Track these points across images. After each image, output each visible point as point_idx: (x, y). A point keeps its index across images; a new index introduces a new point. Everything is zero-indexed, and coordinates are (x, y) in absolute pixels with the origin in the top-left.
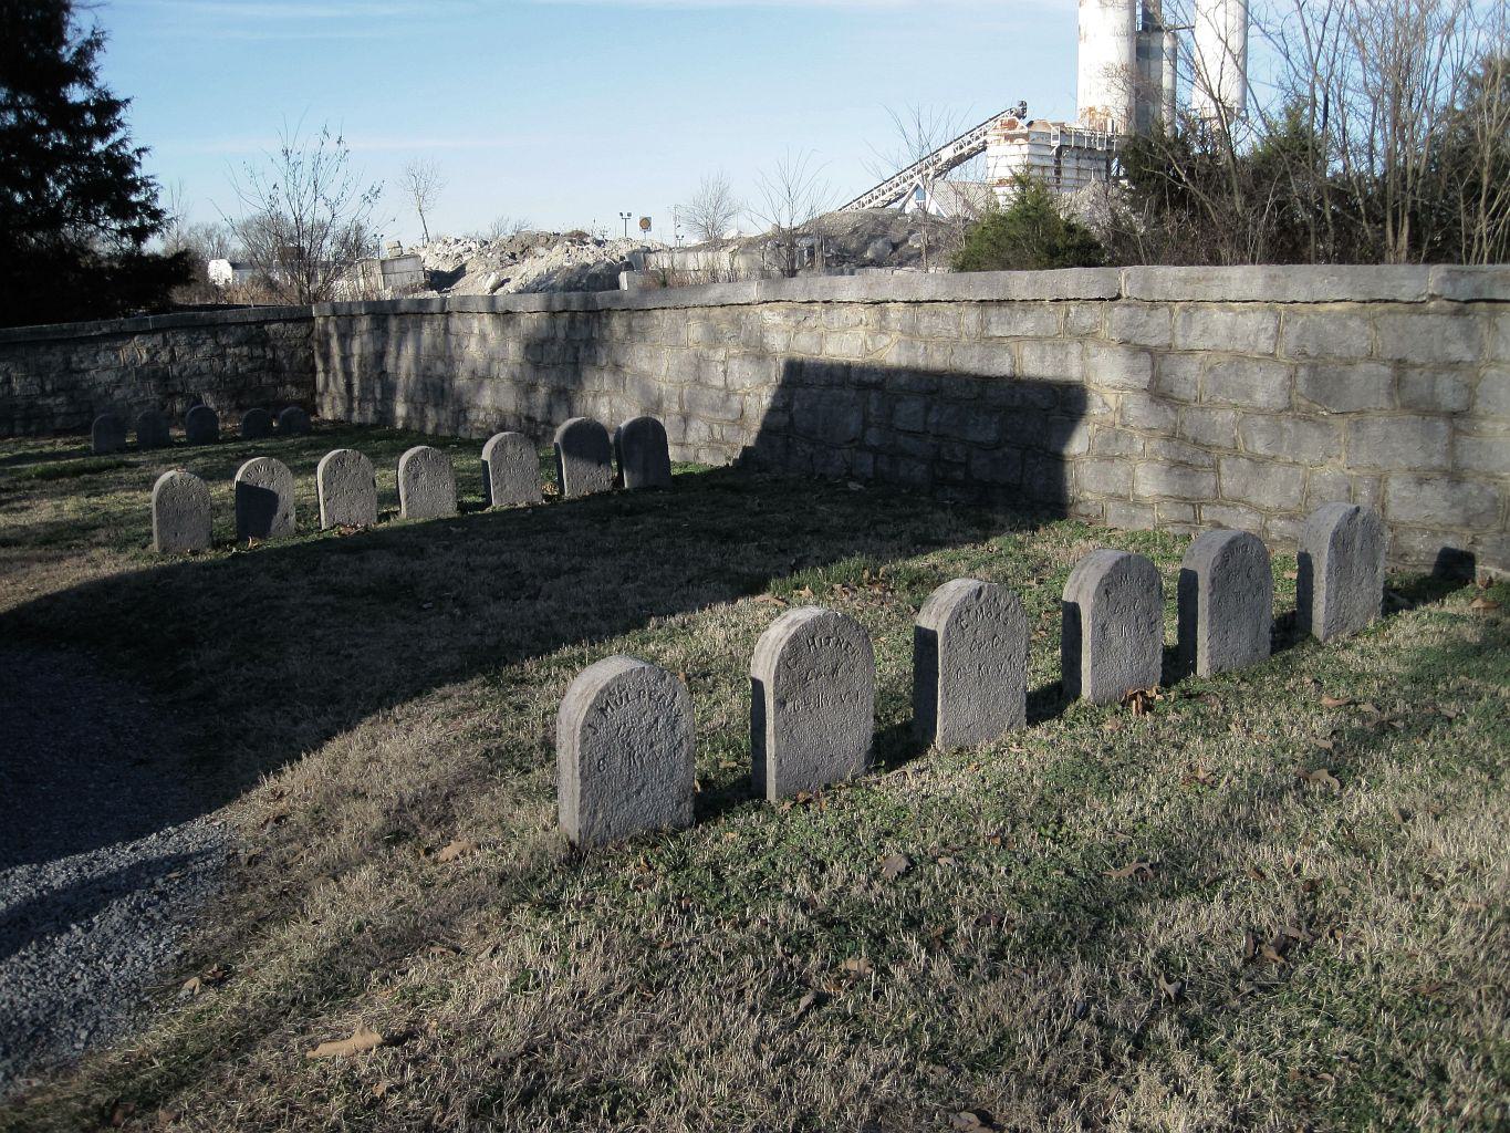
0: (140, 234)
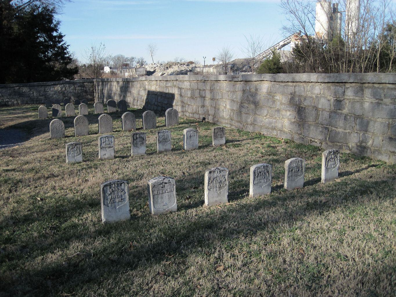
0: (67, 64)
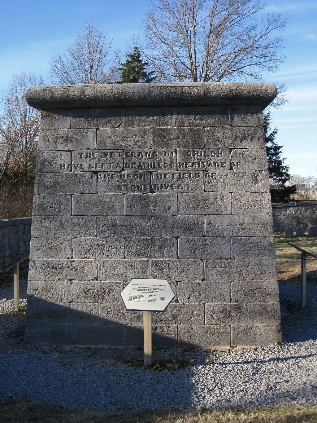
0: (284, 181)
